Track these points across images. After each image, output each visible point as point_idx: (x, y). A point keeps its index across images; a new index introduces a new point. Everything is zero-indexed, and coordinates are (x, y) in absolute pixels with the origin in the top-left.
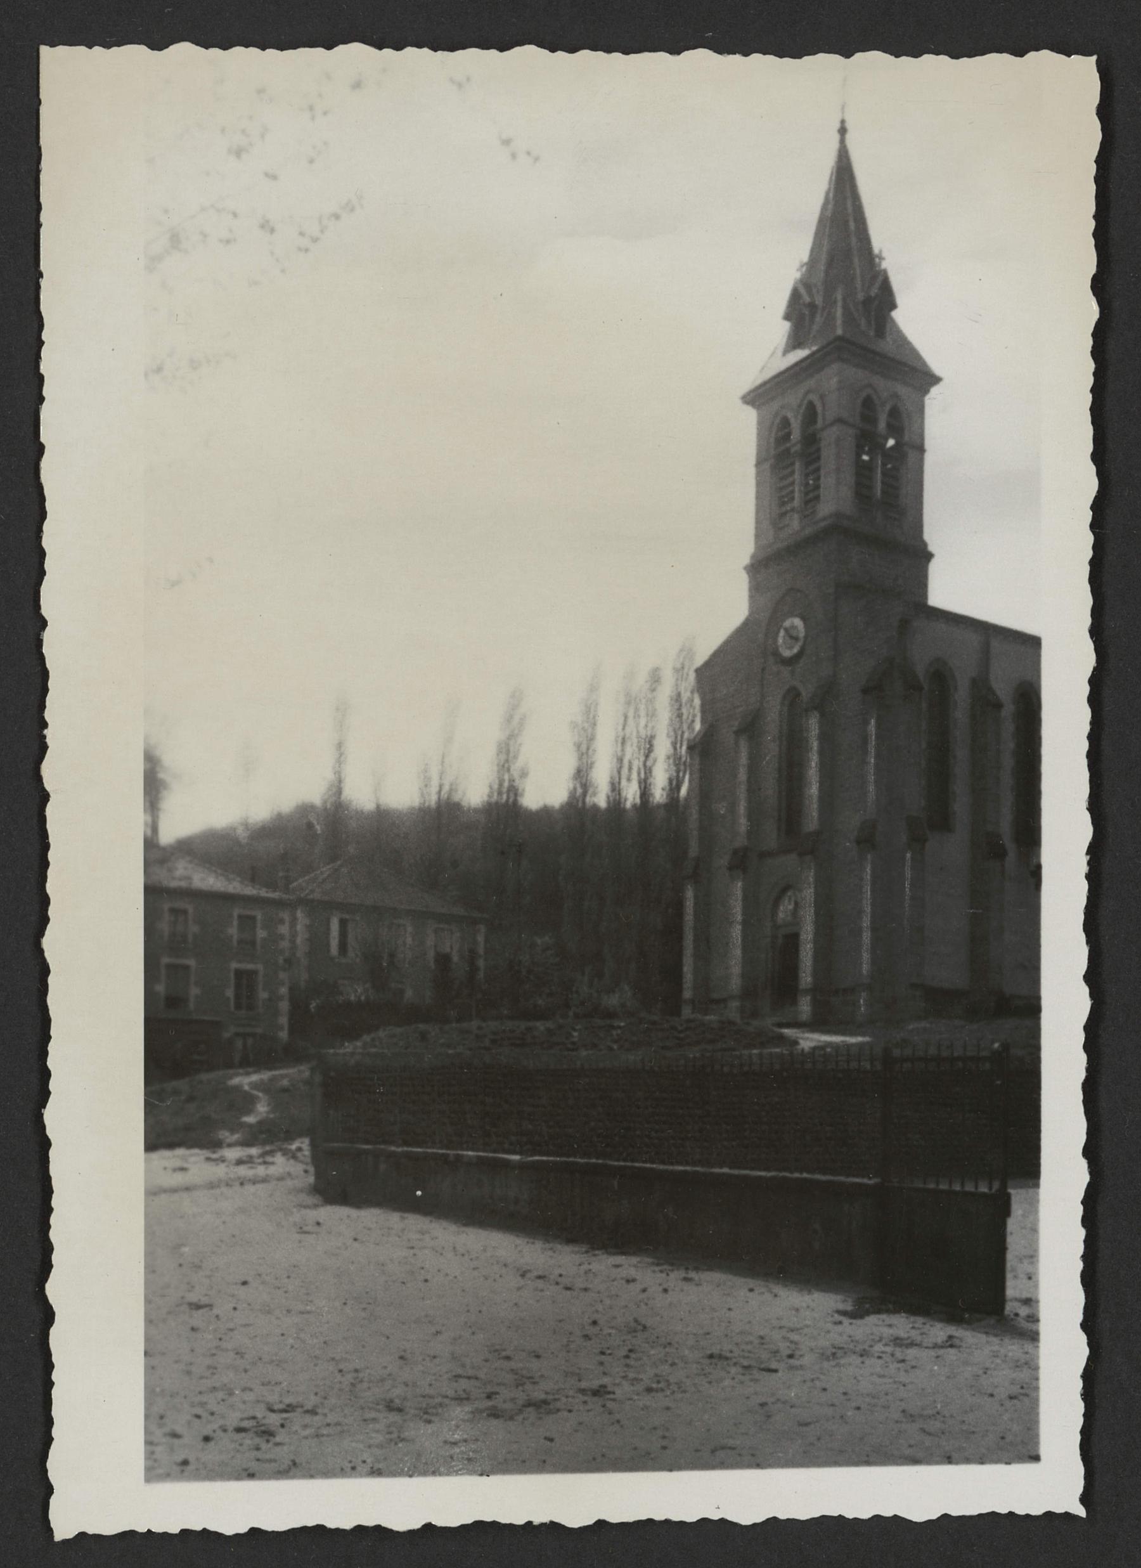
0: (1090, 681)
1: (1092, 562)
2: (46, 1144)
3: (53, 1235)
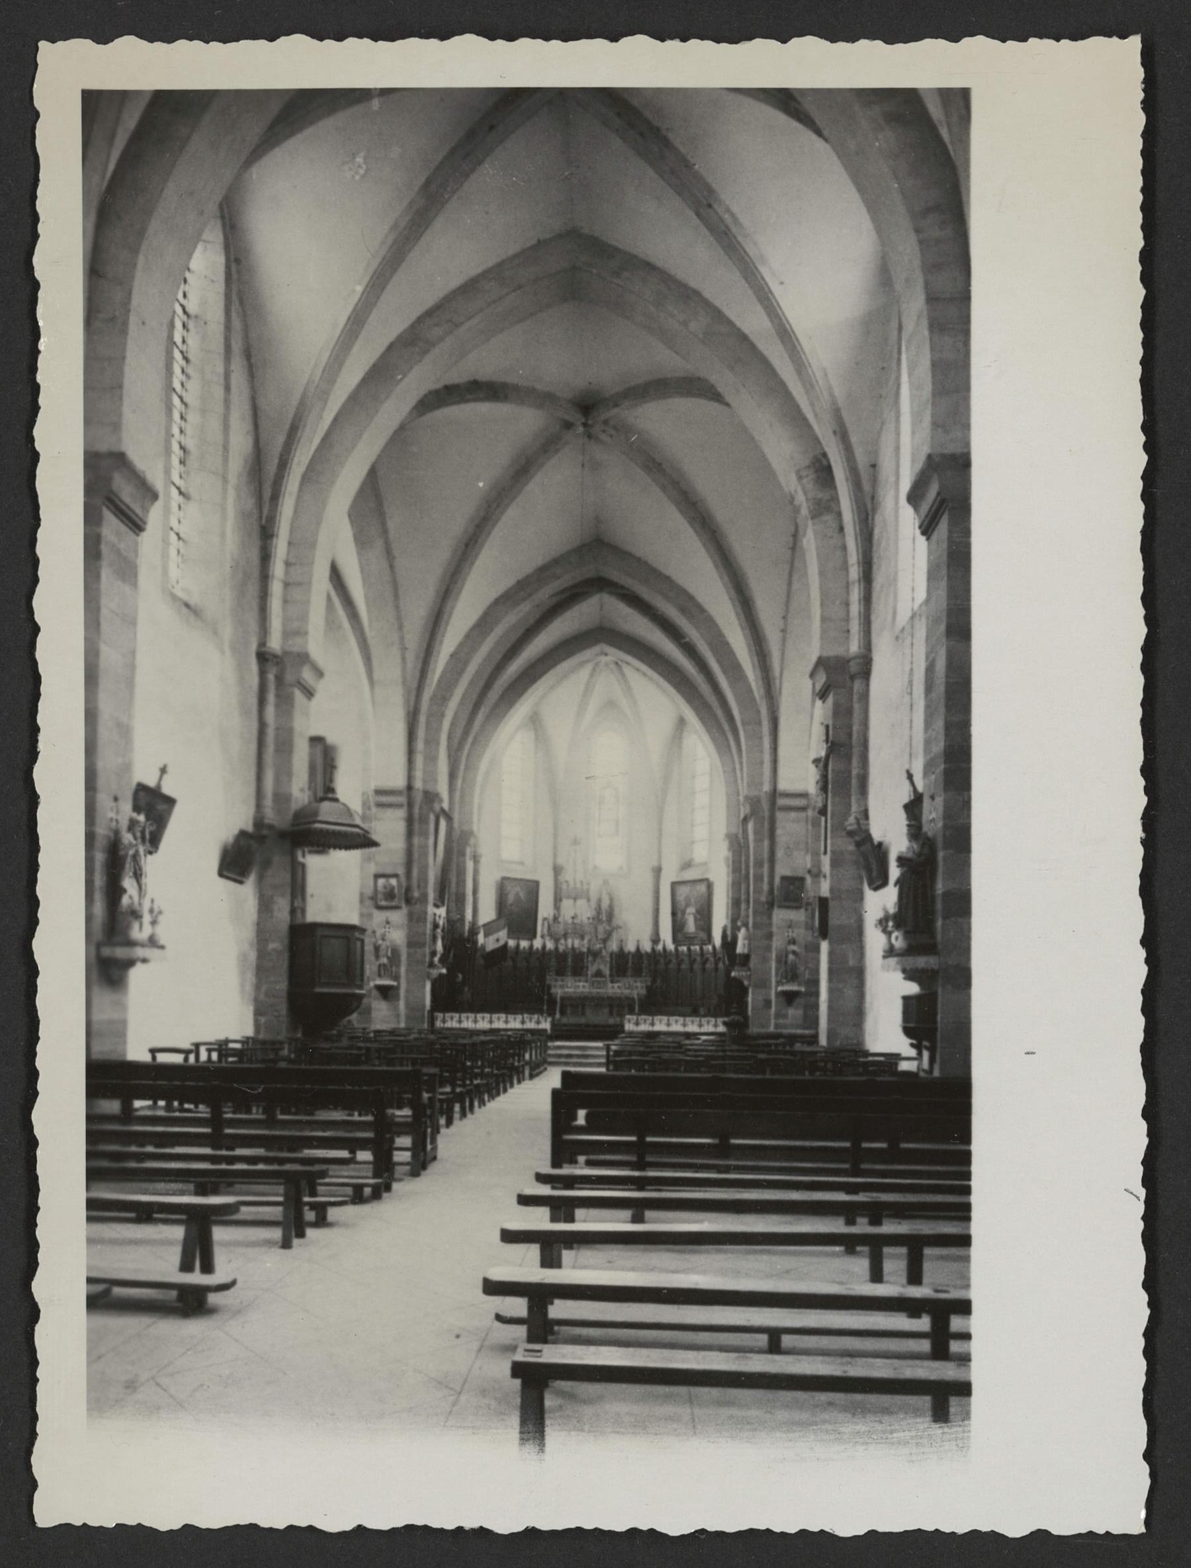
0: (1143, 992)
1: (1144, 532)
2: (33, 1143)
3: (39, 1233)
